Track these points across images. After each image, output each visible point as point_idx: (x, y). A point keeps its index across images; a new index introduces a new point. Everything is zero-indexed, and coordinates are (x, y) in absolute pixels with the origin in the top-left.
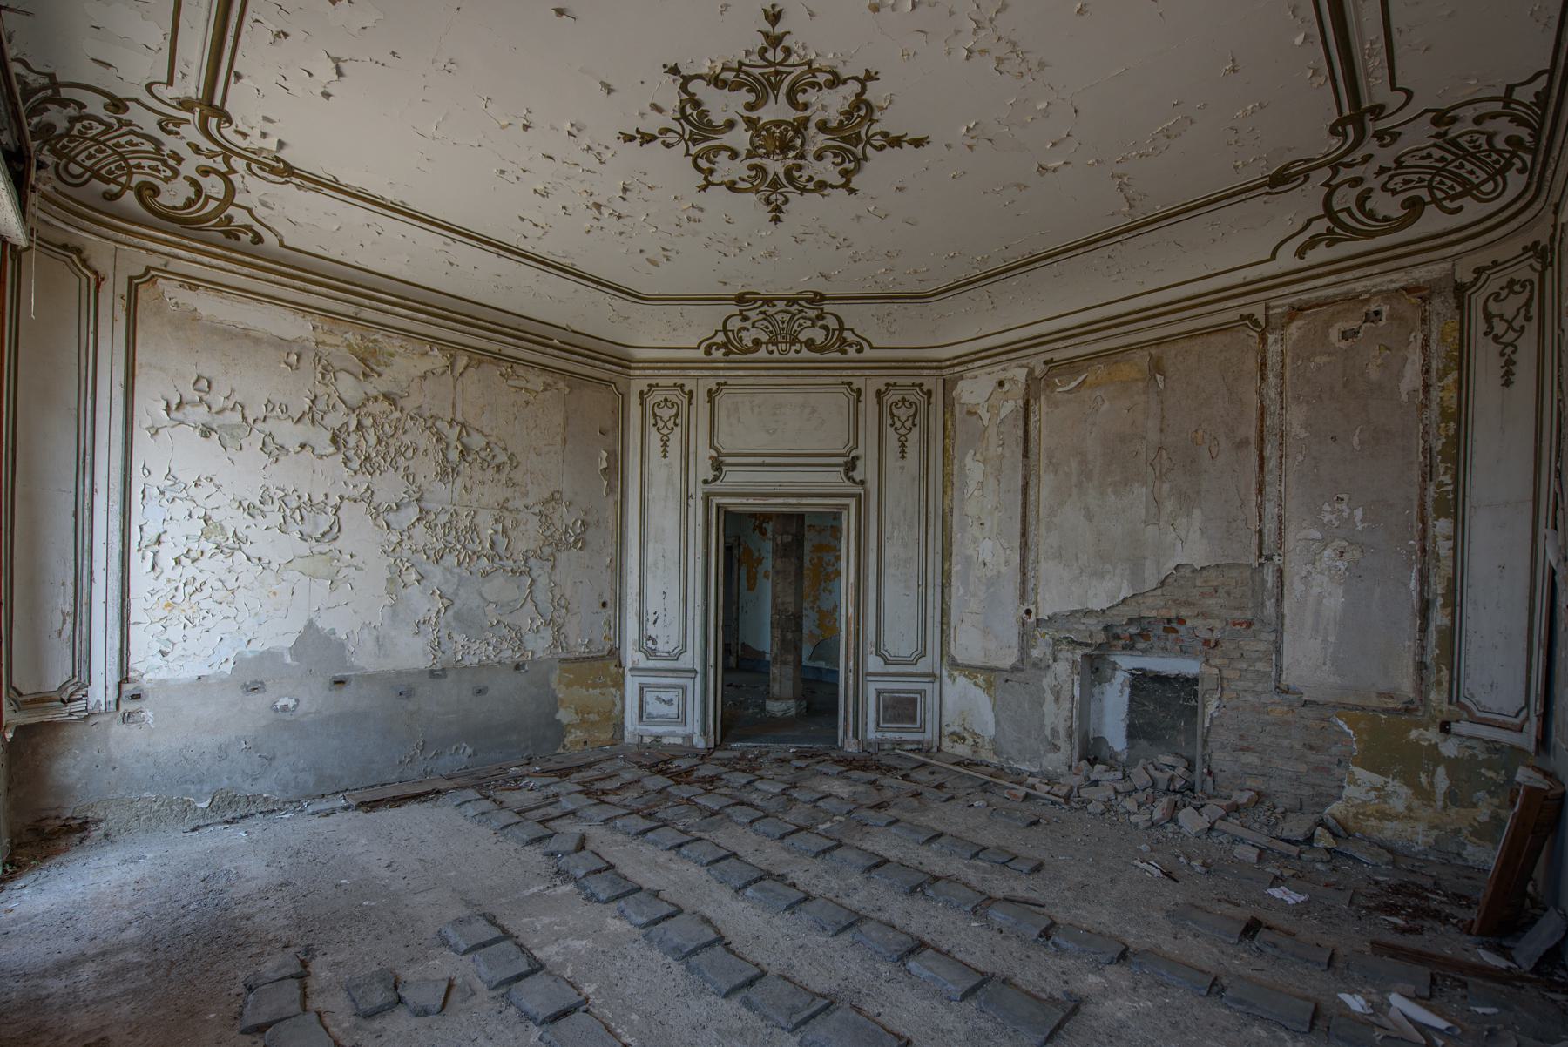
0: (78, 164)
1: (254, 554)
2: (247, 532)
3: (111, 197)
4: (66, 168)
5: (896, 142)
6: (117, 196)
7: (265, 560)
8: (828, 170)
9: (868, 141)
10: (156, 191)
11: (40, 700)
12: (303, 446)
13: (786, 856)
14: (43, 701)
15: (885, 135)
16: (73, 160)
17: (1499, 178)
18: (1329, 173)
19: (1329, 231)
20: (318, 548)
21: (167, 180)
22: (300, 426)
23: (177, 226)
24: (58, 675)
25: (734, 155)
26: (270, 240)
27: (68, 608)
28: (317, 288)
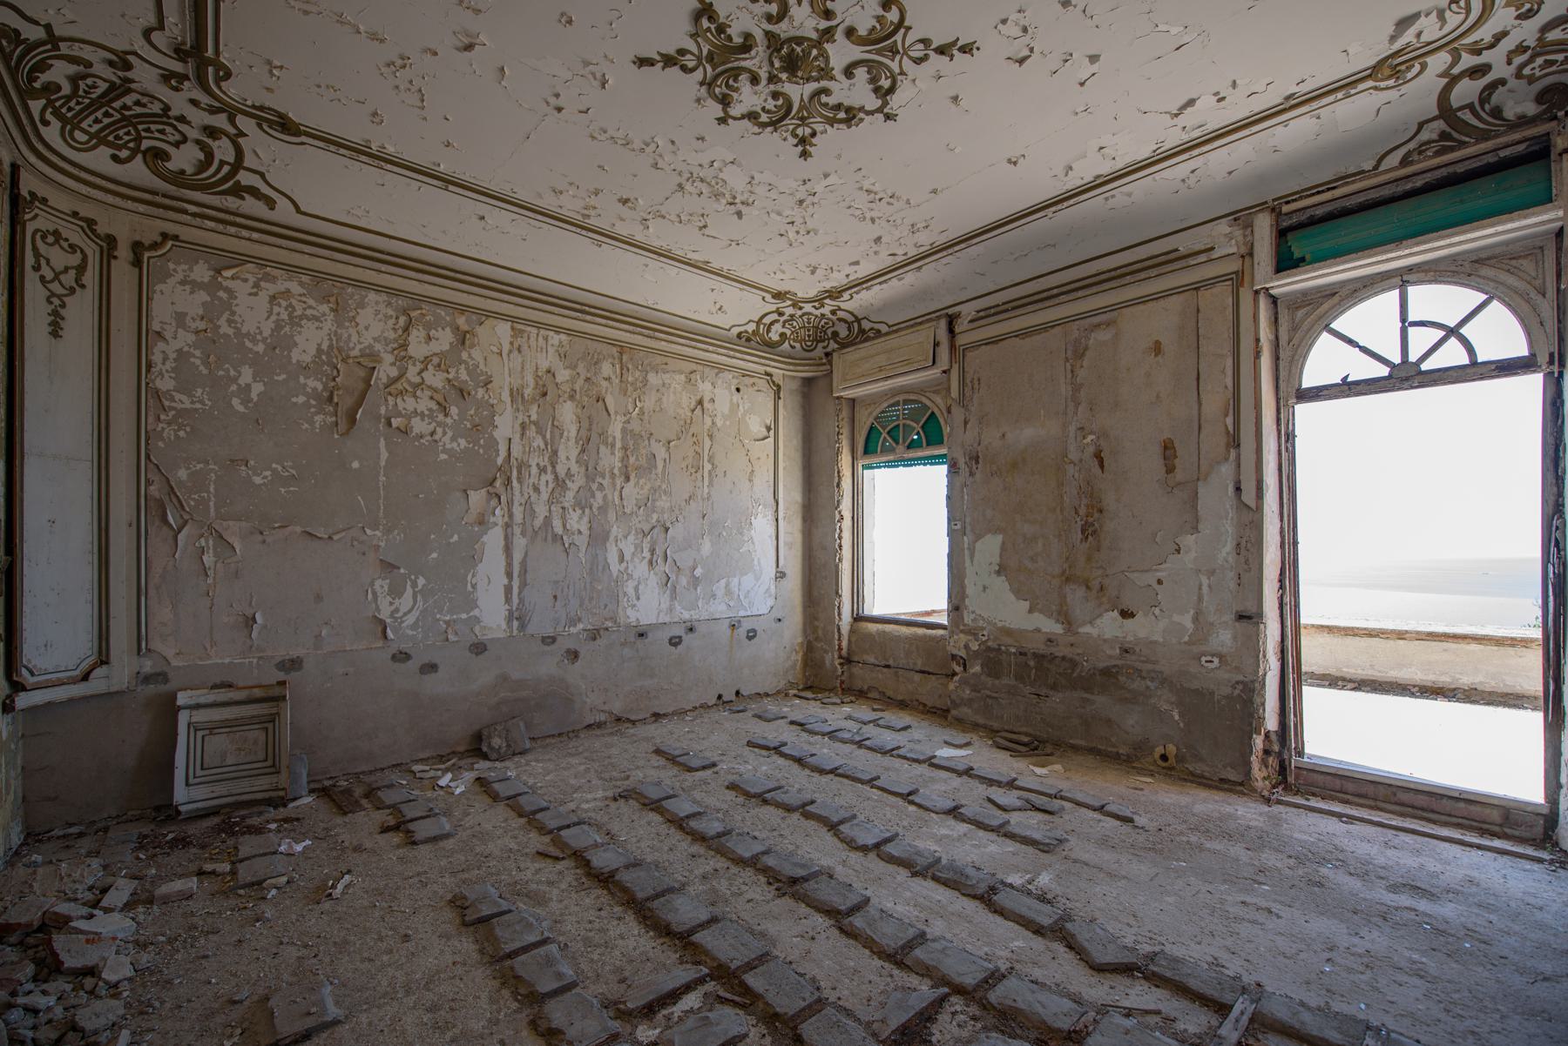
5: (669, 61)
8: (857, 92)
9: (699, 58)
10: (165, 156)
13: (771, 927)
15: (925, 42)
18: (1449, 59)
19: (1444, 136)
21: (177, 145)
23: (1460, 169)
25: (755, 80)
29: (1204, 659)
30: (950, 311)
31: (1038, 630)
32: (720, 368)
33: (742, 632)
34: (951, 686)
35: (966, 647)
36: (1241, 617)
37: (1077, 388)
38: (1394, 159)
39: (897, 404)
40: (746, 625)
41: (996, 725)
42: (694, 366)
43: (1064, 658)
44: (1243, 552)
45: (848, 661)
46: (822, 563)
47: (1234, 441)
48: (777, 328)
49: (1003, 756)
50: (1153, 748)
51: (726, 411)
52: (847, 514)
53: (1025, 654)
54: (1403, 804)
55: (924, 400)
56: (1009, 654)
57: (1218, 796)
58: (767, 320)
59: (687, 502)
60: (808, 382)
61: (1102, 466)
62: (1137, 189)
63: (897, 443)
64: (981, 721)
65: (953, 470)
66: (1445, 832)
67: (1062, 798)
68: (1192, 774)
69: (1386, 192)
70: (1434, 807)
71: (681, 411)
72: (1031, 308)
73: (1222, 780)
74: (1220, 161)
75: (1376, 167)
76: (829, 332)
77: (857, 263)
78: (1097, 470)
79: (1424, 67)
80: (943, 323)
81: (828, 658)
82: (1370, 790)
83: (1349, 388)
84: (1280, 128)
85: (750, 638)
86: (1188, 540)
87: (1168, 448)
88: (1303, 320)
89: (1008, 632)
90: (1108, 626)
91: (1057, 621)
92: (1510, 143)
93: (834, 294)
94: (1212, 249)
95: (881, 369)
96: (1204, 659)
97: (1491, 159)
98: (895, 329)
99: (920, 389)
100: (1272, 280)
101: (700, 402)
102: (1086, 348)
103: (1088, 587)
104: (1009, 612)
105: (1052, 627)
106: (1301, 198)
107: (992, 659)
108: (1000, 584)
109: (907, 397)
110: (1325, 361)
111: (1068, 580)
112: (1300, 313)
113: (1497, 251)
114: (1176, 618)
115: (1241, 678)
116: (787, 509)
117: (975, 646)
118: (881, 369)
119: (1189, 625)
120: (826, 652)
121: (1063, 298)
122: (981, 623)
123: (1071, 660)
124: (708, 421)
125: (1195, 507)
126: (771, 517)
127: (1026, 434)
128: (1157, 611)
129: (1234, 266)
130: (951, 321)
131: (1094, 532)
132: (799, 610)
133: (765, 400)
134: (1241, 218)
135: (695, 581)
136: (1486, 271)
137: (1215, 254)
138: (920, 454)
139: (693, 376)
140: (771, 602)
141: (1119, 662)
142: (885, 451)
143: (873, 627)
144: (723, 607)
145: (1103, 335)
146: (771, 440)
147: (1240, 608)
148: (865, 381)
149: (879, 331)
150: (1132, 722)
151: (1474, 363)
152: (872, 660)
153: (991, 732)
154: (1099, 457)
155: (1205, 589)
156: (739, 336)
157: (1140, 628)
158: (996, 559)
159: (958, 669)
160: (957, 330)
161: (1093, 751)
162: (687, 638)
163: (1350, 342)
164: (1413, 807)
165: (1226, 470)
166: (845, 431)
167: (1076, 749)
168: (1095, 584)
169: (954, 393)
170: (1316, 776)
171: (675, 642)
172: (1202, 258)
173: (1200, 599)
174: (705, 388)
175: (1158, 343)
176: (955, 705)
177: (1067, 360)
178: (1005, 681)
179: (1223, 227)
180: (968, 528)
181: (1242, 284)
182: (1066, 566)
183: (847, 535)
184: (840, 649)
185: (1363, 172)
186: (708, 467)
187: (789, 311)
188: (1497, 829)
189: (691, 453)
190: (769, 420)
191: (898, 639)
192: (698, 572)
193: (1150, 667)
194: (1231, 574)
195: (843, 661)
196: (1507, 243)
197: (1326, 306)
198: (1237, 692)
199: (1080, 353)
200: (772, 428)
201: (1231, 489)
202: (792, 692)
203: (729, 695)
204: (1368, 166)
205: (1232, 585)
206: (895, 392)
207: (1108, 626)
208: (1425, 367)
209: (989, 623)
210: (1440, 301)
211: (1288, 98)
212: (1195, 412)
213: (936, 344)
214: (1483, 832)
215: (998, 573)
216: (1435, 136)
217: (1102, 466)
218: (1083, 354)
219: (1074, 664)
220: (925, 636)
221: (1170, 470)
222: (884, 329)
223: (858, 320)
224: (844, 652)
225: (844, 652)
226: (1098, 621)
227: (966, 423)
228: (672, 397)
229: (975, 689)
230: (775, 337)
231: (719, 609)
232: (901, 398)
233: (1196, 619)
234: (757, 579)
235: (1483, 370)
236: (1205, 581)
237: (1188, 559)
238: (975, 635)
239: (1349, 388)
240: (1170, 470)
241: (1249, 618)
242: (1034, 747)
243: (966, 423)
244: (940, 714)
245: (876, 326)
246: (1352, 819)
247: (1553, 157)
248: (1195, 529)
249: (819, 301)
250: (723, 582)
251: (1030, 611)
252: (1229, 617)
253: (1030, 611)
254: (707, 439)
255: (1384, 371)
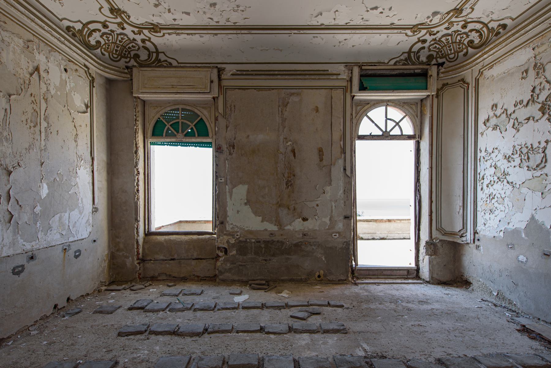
0: (450, 54)
1: (510, 181)
2: (508, 170)
3: (465, 54)
4: (449, 58)
6: (467, 52)
7: (514, 183)
11: (453, 234)
12: (528, 119)
14: (454, 234)
16: (448, 55)
17: (119, 57)
20: (538, 173)
22: (528, 107)
23: (405, 72)
24: (458, 227)
26: (508, 22)
27: (461, 204)
28: (531, 26)
29: (333, 235)
30: (219, 66)
31: (266, 230)
32: (53, 49)
33: (71, 253)
34: (219, 264)
35: (228, 242)
36: (346, 217)
37: (284, 120)
38: (392, 62)
39: (178, 110)
40: (74, 248)
41: (245, 279)
42: (31, 38)
43: (278, 241)
44: (346, 193)
45: (142, 260)
46: (123, 200)
47: (344, 151)
48: (96, 36)
49: (261, 293)
50: (315, 274)
51: (58, 84)
52: (141, 171)
53: (259, 242)
54: (385, 275)
55: (196, 111)
56: (251, 243)
57: (339, 287)
58: (92, 27)
59: (28, 149)
60: (109, 82)
61: (295, 156)
62: (340, 36)
63: (178, 132)
64: (236, 278)
65: (218, 151)
66: (372, 281)
67: (311, 305)
68: (329, 280)
69: (387, 72)
70: (392, 274)
71: (20, 71)
72: (263, 77)
73: (339, 280)
74: (357, 40)
75: (388, 63)
76: (132, 53)
77: (188, 14)
78: (292, 158)
79: (420, 31)
80: (215, 71)
81: (129, 262)
82: (376, 273)
83: (371, 137)
84: (378, 35)
85: (76, 257)
86: (328, 188)
87: (320, 151)
88: (411, 108)
89: (251, 232)
90: (297, 225)
91: (275, 225)
92: (417, 68)
93: (155, 28)
94: (339, 74)
95: (173, 87)
96: (333, 235)
97: (412, 72)
98: (182, 66)
99: (194, 104)
100: (358, 93)
101: (37, 69)
102: (288, 103)
103: (289, 209)
104: (248, 222)
105: (272, 228)
106: (366, 65)
107: (243, 246)
108: (247, 209)
109: (184, 107)
110: (365, 127)
111: (280, 206)
112: (359, 108)
113: (409, 101)
114: (324, 220)
115: (345, 240)
116: (98, 164)
117: (232, 241)
118: (173, 87)
119: (328, 222)
120: (127, 257)
121: (279, 77)
122: (236, 229)
123: (281, 242)
124: (44, 87)
125: (330, 175)
126: (89, 169)
127: (261, 137)
128: (317, 217)
129: (345, 84)
130: (220, 71)
131: (291, 184)
132: (106, 232)
133: (84, 84)
134: (349, 66)
135: (35, 217)
136: (406, 106)
137: (340, 77)
138: (194, 140)
139: (30, 44)
140: (89, 229)
141: (302, 240)
142: (168, 135)
143: (160, 238)
144: (58, 236)
145: (295, 99)
146: (88, 114)
147: (345, 214)
148: (157, 92)
149: (171, 64)
150: (307, 264)
151: (402, 135)
152: (162, 257)
153: (244, 283)
154: (293, 151)
155: (334, 207)
156: (68, 28)
157: (310, 225)
158: (244, 197)
159: (221, 254)
160: (223, 77)
161: (291, 280)
162: (30, 266)
163: (373, 122)
164: (387, 275)
165: (341, 162)
166: (140, 119)
167: (283, 281)
168: (292, 207)
169: (221, 110)
170: (362, 272)
171: (18, 271)
172: (335, 77)
173: (332, 212)
174: (41, 59)
175: (317, 107)
176: (221, 273)
177: (279, 106)
178: (249, 256)
179: (342, 68)
180: (229, 181)
181: (347, 91)
182: (279, 200)
183: (141, 183)
184: (138, 252)
185: (384, 63)
186: (44, 124)
187: (112, 27)
188: (406, 277)
189: (30, 110)
190: (87, 100)
191: (181, 243)
192: (38, 209)
193: (314, 240)
194: (342, 202)
195: (138, 258)
196: (410, 99)
197: (366, 107)
198: (344, 246)
199: (286, 105)
200: (89, 106)
201: (342, 169)
202: (104, 288)
203: (62, 303)
204: (386, 61)
205: (343, 205)
206: (176, 102)
207: (297, 225)
208: (391, 133)
209: (241, 229)
210: (395, 114)
211: (392, 24)
212: (330, 138)
213: (212, 82)
214: (405, 279)
215: (246, 204)
216: (404, 59)
217: (295, 156)
218: (287, 105)
219: (282, 243)
220: (198, 239)
221: (321, 160)
222: (175, 63)
223: (157, 52)
224: (141, 256)
225: (141, 256)
226: (293, 223)
227: (227, 127)
228: (11, 56)
229: (233, 263)
230: (93, 42)
231: (55, 238)
232: (180, 107)
233: (330, 219)
234: (81, 213)
235: (405, 137)
236: (334, 205)
237: (328, 196)
238: (233, 235)
239: (371, 137)
240: (321, 160)
241: (348, 217)
242: (267, 284)
243: (227, 127)
244: (212, 279)
245: (169, 60)
246: (379, 284)
247: (428, 76)
248: (330, 184)
249: (140, 29)
250: (57, 217)
251: (262, 221)
252: (342, 218)
253: (262, 221)
254: (43, 101)
255: (380, 133)
